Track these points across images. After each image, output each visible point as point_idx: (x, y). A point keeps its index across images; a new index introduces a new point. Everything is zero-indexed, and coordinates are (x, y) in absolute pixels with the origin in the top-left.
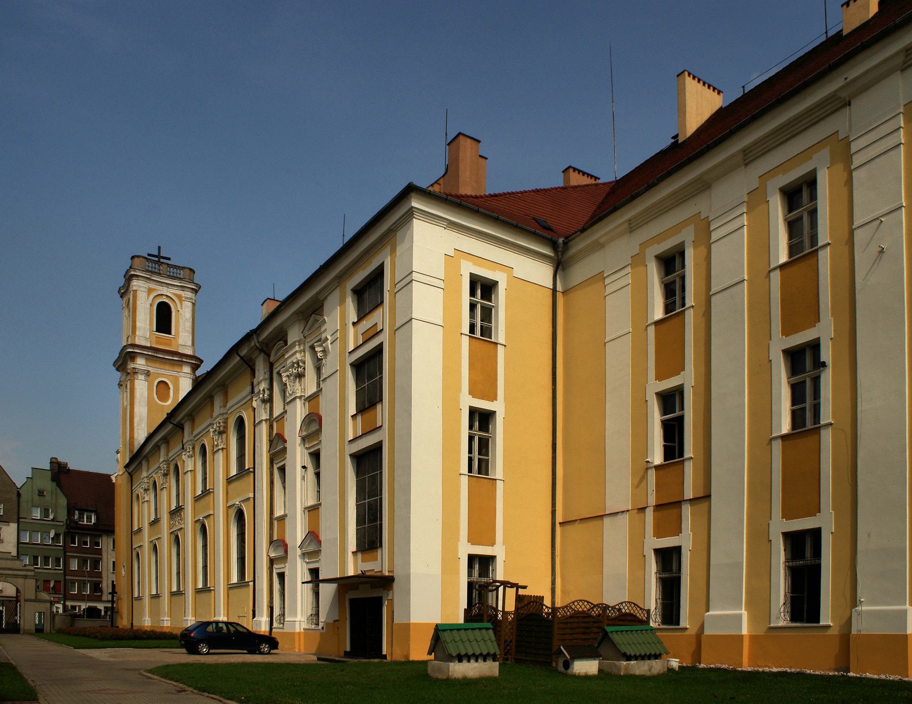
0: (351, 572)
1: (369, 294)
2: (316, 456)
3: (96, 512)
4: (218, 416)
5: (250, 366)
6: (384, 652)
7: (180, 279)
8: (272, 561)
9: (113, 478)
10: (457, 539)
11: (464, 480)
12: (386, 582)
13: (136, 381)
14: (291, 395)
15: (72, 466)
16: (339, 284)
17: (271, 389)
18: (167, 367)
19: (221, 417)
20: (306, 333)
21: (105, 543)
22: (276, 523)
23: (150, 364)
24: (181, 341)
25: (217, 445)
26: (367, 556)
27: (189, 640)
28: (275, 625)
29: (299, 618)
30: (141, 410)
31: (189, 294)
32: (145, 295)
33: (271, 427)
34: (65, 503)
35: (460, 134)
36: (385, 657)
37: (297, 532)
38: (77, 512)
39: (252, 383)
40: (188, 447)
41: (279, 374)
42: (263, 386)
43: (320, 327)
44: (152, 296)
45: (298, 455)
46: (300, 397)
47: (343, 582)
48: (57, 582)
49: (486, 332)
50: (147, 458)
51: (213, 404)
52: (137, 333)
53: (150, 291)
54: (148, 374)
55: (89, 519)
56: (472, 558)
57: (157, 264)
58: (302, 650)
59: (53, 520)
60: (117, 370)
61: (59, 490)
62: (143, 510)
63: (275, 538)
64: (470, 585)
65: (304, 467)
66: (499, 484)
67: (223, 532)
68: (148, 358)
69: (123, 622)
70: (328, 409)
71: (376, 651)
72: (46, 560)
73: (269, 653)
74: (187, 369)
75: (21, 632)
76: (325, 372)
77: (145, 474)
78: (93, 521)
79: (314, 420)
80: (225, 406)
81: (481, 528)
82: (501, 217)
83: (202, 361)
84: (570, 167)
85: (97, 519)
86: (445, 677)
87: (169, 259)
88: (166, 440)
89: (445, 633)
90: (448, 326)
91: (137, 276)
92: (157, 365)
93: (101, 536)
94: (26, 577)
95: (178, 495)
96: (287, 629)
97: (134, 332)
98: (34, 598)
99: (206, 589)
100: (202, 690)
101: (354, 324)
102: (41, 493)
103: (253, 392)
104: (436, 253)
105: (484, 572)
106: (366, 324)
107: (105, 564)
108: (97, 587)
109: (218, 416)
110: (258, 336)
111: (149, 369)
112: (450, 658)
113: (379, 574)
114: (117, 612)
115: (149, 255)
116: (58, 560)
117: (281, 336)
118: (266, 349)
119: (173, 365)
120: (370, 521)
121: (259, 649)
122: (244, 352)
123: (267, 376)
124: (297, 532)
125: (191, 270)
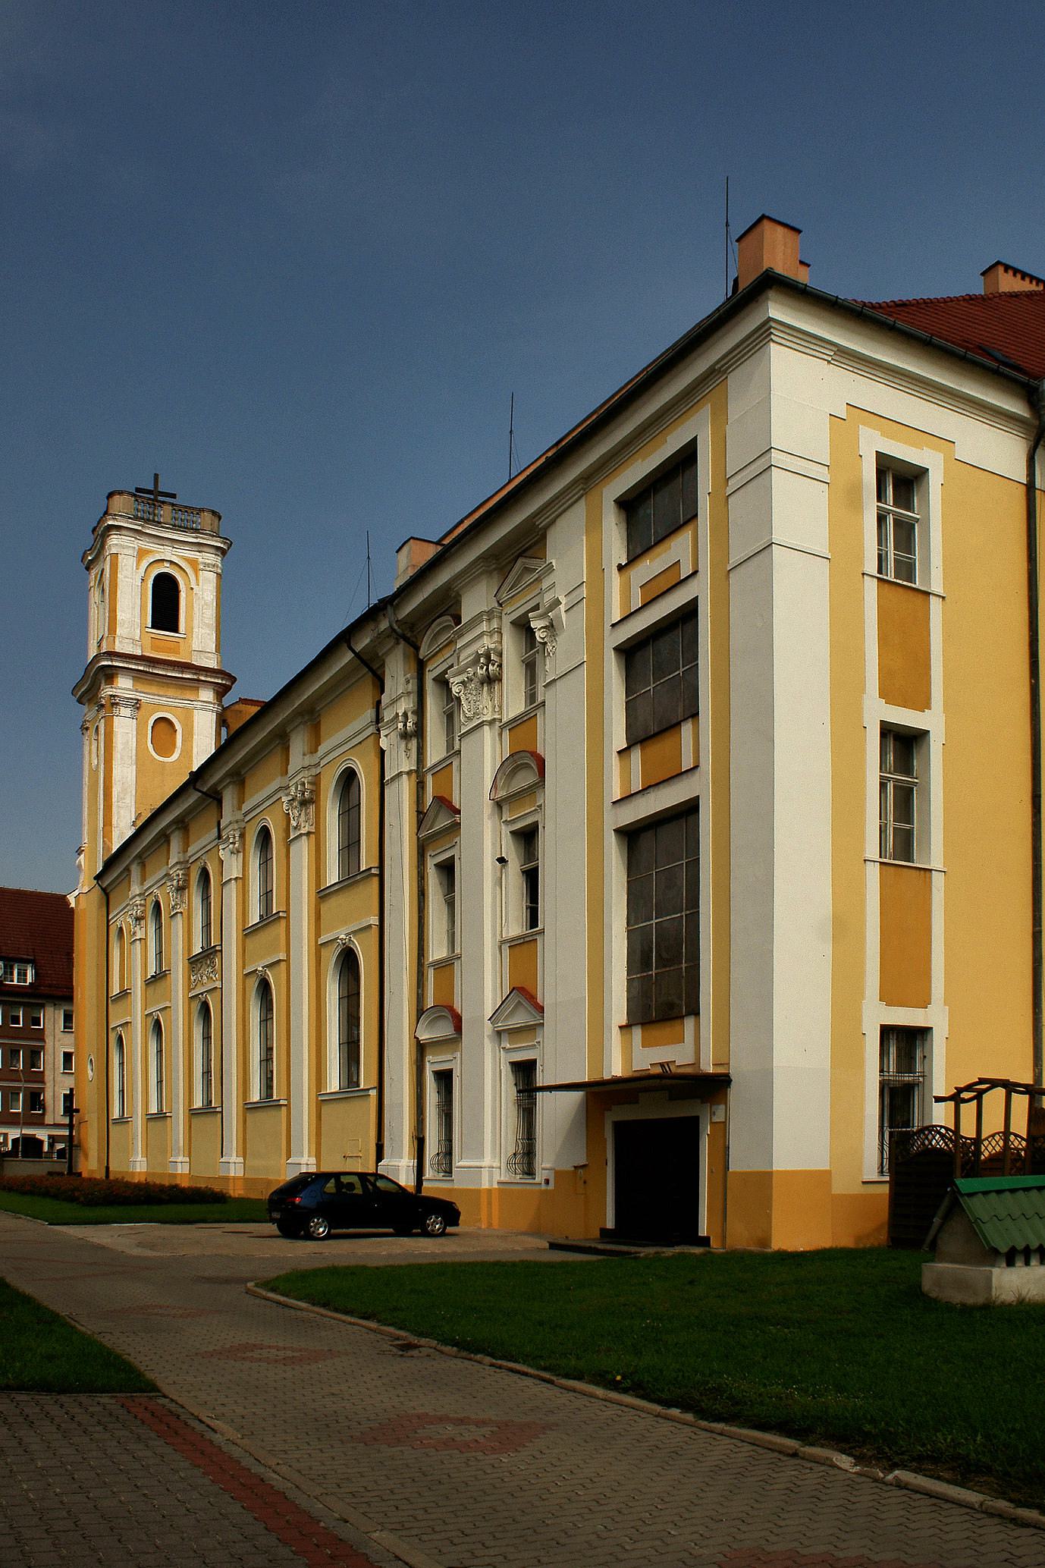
0: (616, 1068)
1: (659, 506)
2: (527, 837)
3: (33, 962)
4: (298, 772)
5: (371, 669)
6: (703, 1232)
7: (196, 531)
8: (421, 1049)
9: (71, 899)
10: (859, 993)
11: (873, 872)
12: (714, 1087)
14: (469, 719)
16: (586, 492)
17: (420, 710)
18: (171, 692)
19: (306, 773)
20: (504, 596)
21: (51, 1018)
22: (431, 973)
24: (196, 645)
26: (657, 1032)
27: (296, 1206)
28: (428, 1173)
29: (487, 1161)
30: (124, 772)
31: (211, 558)
33: (421, 785)
35: (763, 217)
36: (705, 1241)
37: (484, 989)
39: (379, 702)
40: (231, 833)
41: (443, 682)
42: (406, 705)
43: (538, 580)
44: (144, 564)
45: (485, 839)
46: (492, 722)
47: (596, 1089)
49: (906, 569)
50: (142, 859)
51: (287, 749)
53: (141, 554)
54: (137, 705)
55: (22, 975)
56: (886, 1031)
57: (153, 502)
58: (495, 1222)
60: (79, 701)
62: (128, 959)
63: (430, 1003)
64: (883, 1085)
65: (502, 860)
66: (938, 880)
67: (309, 997)
68: (138, 676)
69: (90, 1165)
70: (561, 740)
71: (688, 1232)
73: (443, 1234)
74: (207, 695)
76: (550, 669)
77: (136, 889)
78: (29, 980)
79: (526, 765)
81: (905, 975)
82: (936, 340)
83: (234, 680)
84: (998, 263)
85: (37, 975)
86: (981, 1300)
87: (174, 496)
88: (182, 824)
89: (975, 1199)
90: (839, 559)
92: (154, 689)
93: (43, 1006)
95: (207, 926)
96: (460, 1181)
97: (112, 629)
100: (469, 1347)
101: (620, 568)
103: (378, 719)
104: (812, 406)
105: (907, 1060)
106: (650, 567)
107: (49, 1058)
108: (35, 1100)
109: (298, 772)
110: (397, 608)
111: (139, 696)
112: (992, 1255)
113: (689, 1070)
114: (79, 1146)
115: (138, 490)
117: (447, 605)
118: (409, 635)
119: (183, 687)
120: (662, 962)
121: (424, 1227)
122: (362, 643)
123: (412, 686)
124: (484, 989)
125: (214, 513)
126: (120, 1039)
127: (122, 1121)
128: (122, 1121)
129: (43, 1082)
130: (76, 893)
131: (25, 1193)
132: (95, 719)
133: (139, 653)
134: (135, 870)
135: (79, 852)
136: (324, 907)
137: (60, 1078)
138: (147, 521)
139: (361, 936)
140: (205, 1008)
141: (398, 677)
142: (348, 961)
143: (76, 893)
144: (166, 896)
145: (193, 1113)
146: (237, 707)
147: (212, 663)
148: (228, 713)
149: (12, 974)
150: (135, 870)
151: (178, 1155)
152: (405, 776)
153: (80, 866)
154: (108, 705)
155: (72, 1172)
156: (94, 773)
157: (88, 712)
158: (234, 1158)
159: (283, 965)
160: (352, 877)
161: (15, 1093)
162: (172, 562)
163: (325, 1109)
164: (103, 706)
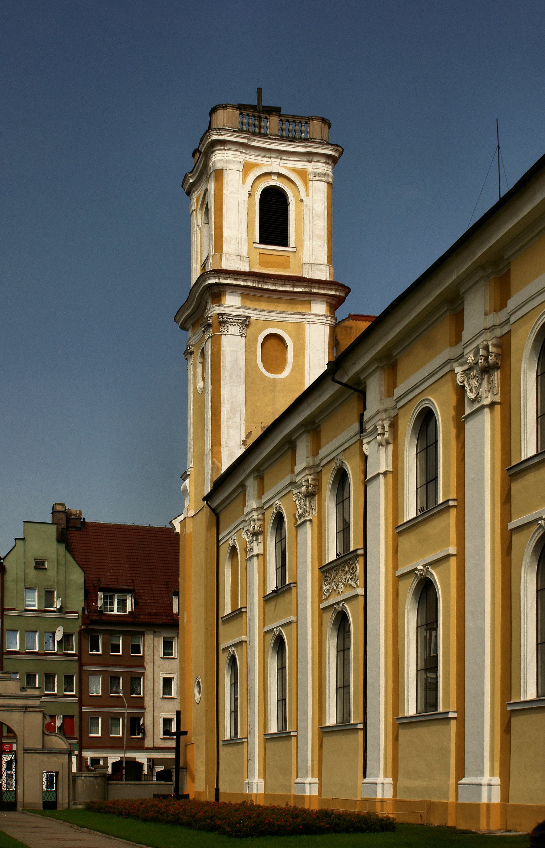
7: (306, 140)
13: (224, 339)
15: (89, 517)
18: (282, 307)
21: (151, 646)
23: (249, 304)
24: (306, 257)
25: (301, 516)
30: (233, 392)
31: (322, 167)
32: (238, 176)
34: (82, 580)
38: (100, 594)
44: (251, 178)
48: (68, 718)
50: (259, 474)
52: (225, 249)
53: (247, 168)
54: (246, 322)
55: (122, 604)
57: (259, 116)
59: (60, 610)
61: (69, 557)
62: (251, 576)
68: (247, 293)
72: (49, 678)
74: (320, 308)
75: (19, 808)
77: (252, 504)
78: (129, 608)
80: (390, 394)
83: (347, 290)
85: (136, 604)
91: (223, 143)
92: (264, 305)
93: (142, 634)
94: (25, 709)
98: (40, 747)
99: (283, 736)
102: (39, 565)
103: (362, 430)
108: (136, 725)
111: (248, 313)
116: (68, 679)
126: (233, 661)
127: (235, 741)
128: (235, 741)
129: (143, 707)
130: (181, 518)
131: (146, 820)
132: (200, 342)
133: (247, 269)
134: (252, 486)
135: (185, 476)
136: (516, 487)
137: (159, 703)
138: (254, 134)
139: (286, 628)
140: (342, 622)
141: (477, 314)
142: (342, 622)
143: (181, 518)
144: (290, 506)
145: (325, 732)
146: (347, 323)
147: (324, 274)
148: (338, 330)
149: (112, 604)
150: (252, 486)
151: (306, 775)
152: (382, 477)
153: (185, 490)
154: (216, 324)
155: (180, 796)
156: (200, 396)
157: (193, 337)
158: (381, 779)
159: (294, 625)
160: (430, 509)
161: (115, 719)
162: (280, 175)
163: (516, 721)
164: (210, 325)
